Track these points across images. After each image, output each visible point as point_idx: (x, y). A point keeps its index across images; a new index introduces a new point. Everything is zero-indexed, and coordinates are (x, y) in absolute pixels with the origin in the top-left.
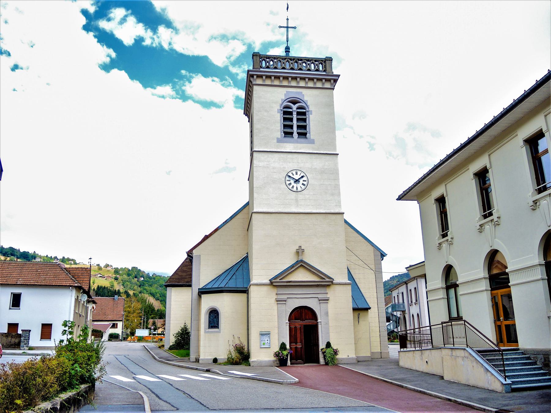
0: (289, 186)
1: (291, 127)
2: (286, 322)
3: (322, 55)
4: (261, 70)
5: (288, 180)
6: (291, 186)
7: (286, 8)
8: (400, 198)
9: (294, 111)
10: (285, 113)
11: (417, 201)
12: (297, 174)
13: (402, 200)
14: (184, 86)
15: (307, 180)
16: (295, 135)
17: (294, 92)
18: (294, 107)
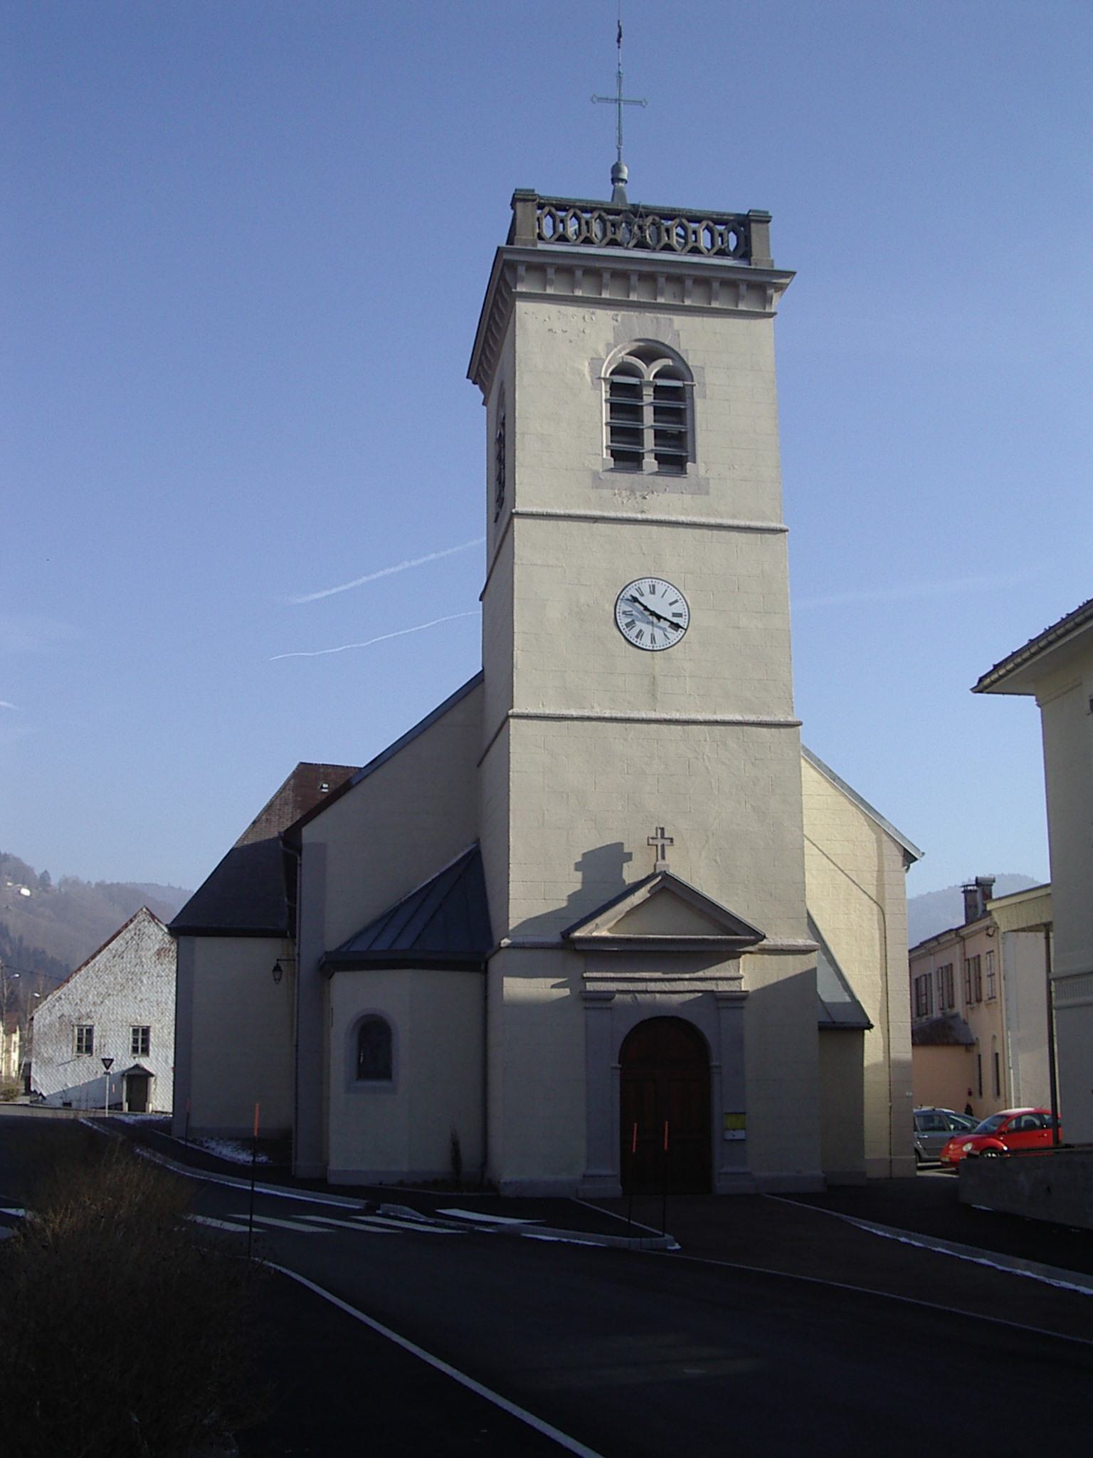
0: (627, 630)
1: (636, 435)
2: (614, 1065)
3: (737, 206)
4: (541, 246)
5: (624, 613)
6: (635, 631)
7: (616, 38)
8: (984, 686)
9: (649, 384)
10: (615, 388)
11: (1034, 697)
12: (653, 592)
13: (988, 693)
14: (966, 1049)
15: (681, 597)
16: (650, 462)
17: (647, 326)
18: (650, 372)
